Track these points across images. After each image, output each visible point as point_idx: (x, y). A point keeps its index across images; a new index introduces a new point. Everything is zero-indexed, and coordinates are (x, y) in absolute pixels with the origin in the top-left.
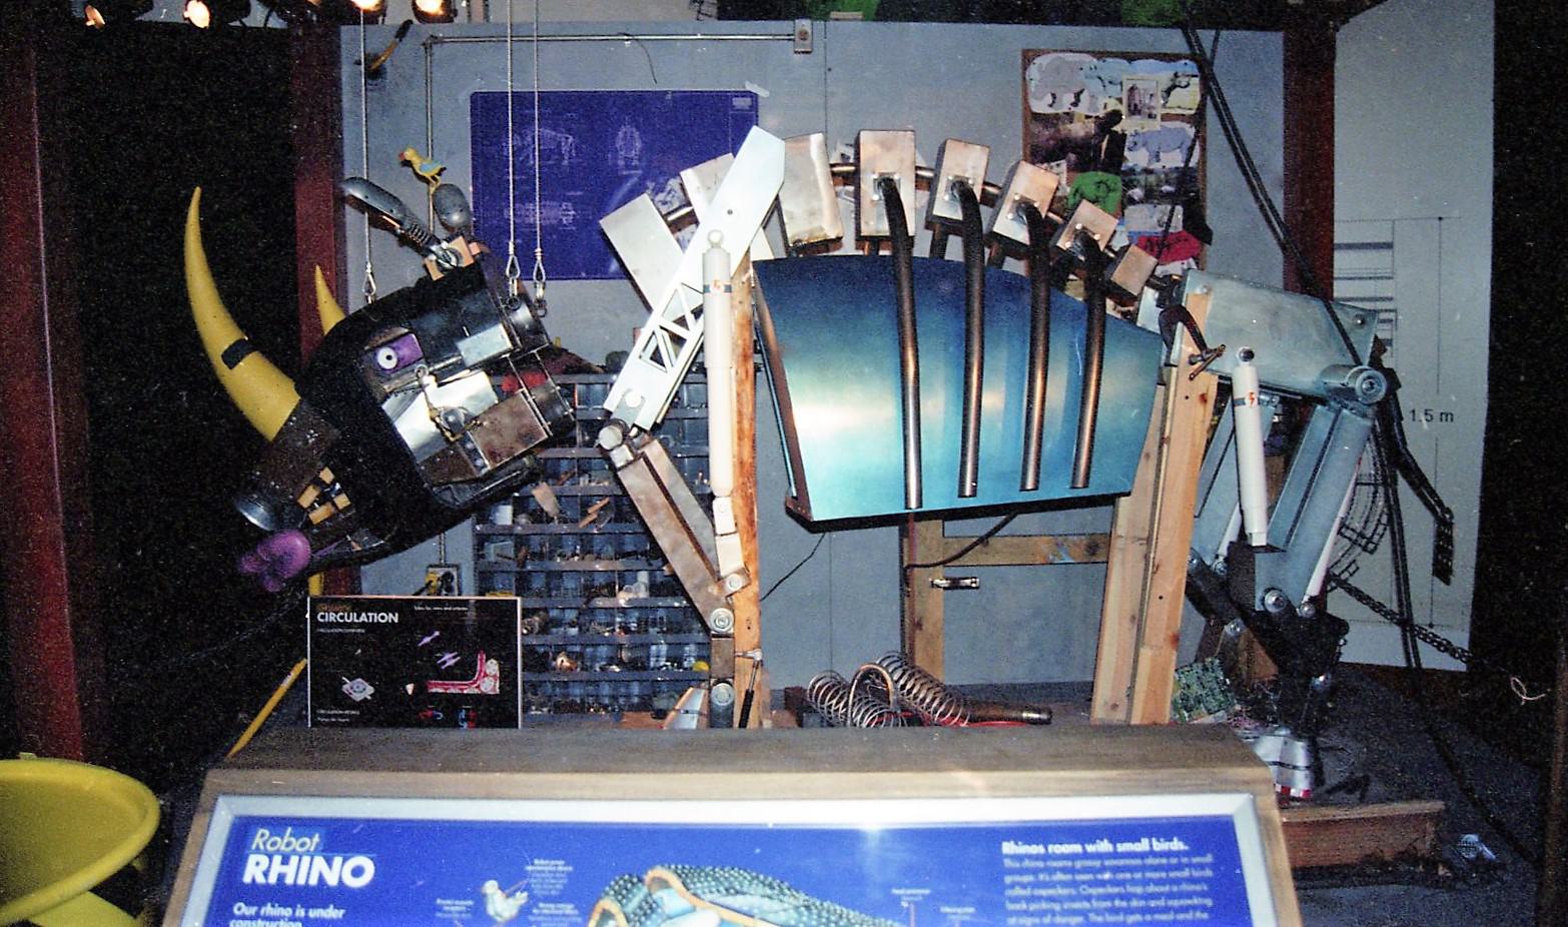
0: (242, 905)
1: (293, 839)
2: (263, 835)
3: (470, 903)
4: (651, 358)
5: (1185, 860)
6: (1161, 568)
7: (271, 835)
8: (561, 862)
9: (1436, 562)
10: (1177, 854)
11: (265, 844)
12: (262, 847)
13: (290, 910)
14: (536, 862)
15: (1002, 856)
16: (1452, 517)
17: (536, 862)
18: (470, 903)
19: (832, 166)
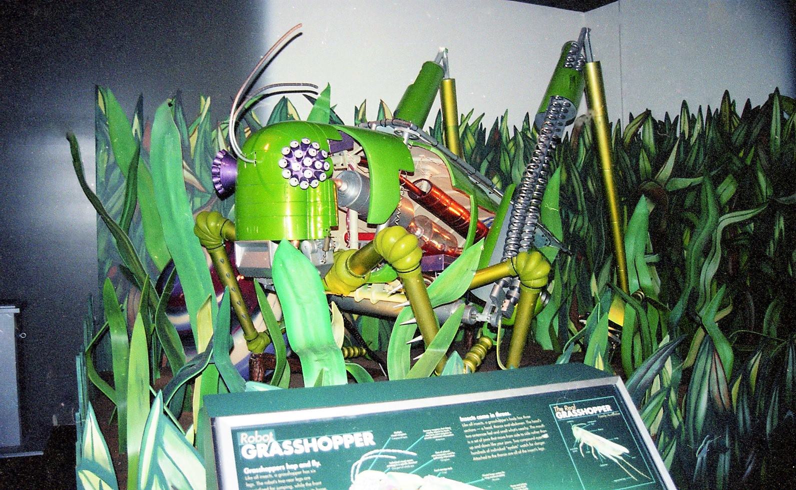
0: (248, 468)
1: (260, 436)
2: (244, 436)
3: (595, 421)
4: (359, 233)
5: (511, 419)
6: (520, 272)
7: (249, 436)
8: (401, 432)
9: (454, 82)
10: (507, 417)
11: (247, 439)
12: (246, 441)
13: (283, 467)
14: (395, 433)
15: (461, 423)
16: (701, 318)
17: (395, 433)
18: (595, 421)
19: (403, 172)
